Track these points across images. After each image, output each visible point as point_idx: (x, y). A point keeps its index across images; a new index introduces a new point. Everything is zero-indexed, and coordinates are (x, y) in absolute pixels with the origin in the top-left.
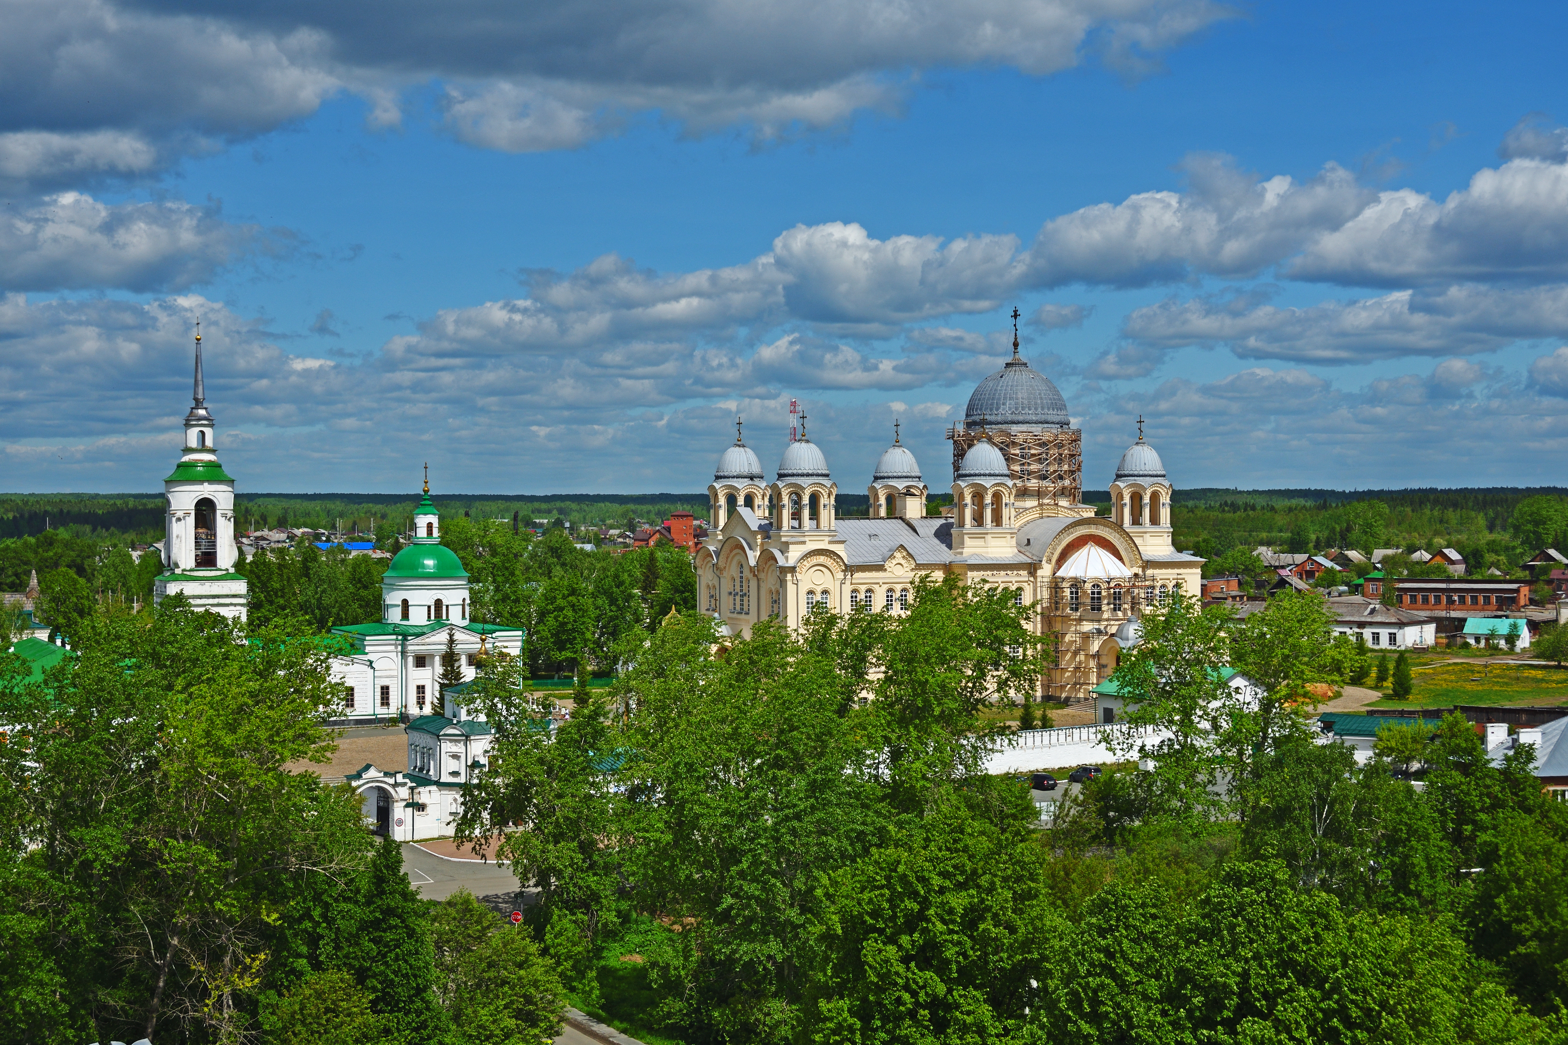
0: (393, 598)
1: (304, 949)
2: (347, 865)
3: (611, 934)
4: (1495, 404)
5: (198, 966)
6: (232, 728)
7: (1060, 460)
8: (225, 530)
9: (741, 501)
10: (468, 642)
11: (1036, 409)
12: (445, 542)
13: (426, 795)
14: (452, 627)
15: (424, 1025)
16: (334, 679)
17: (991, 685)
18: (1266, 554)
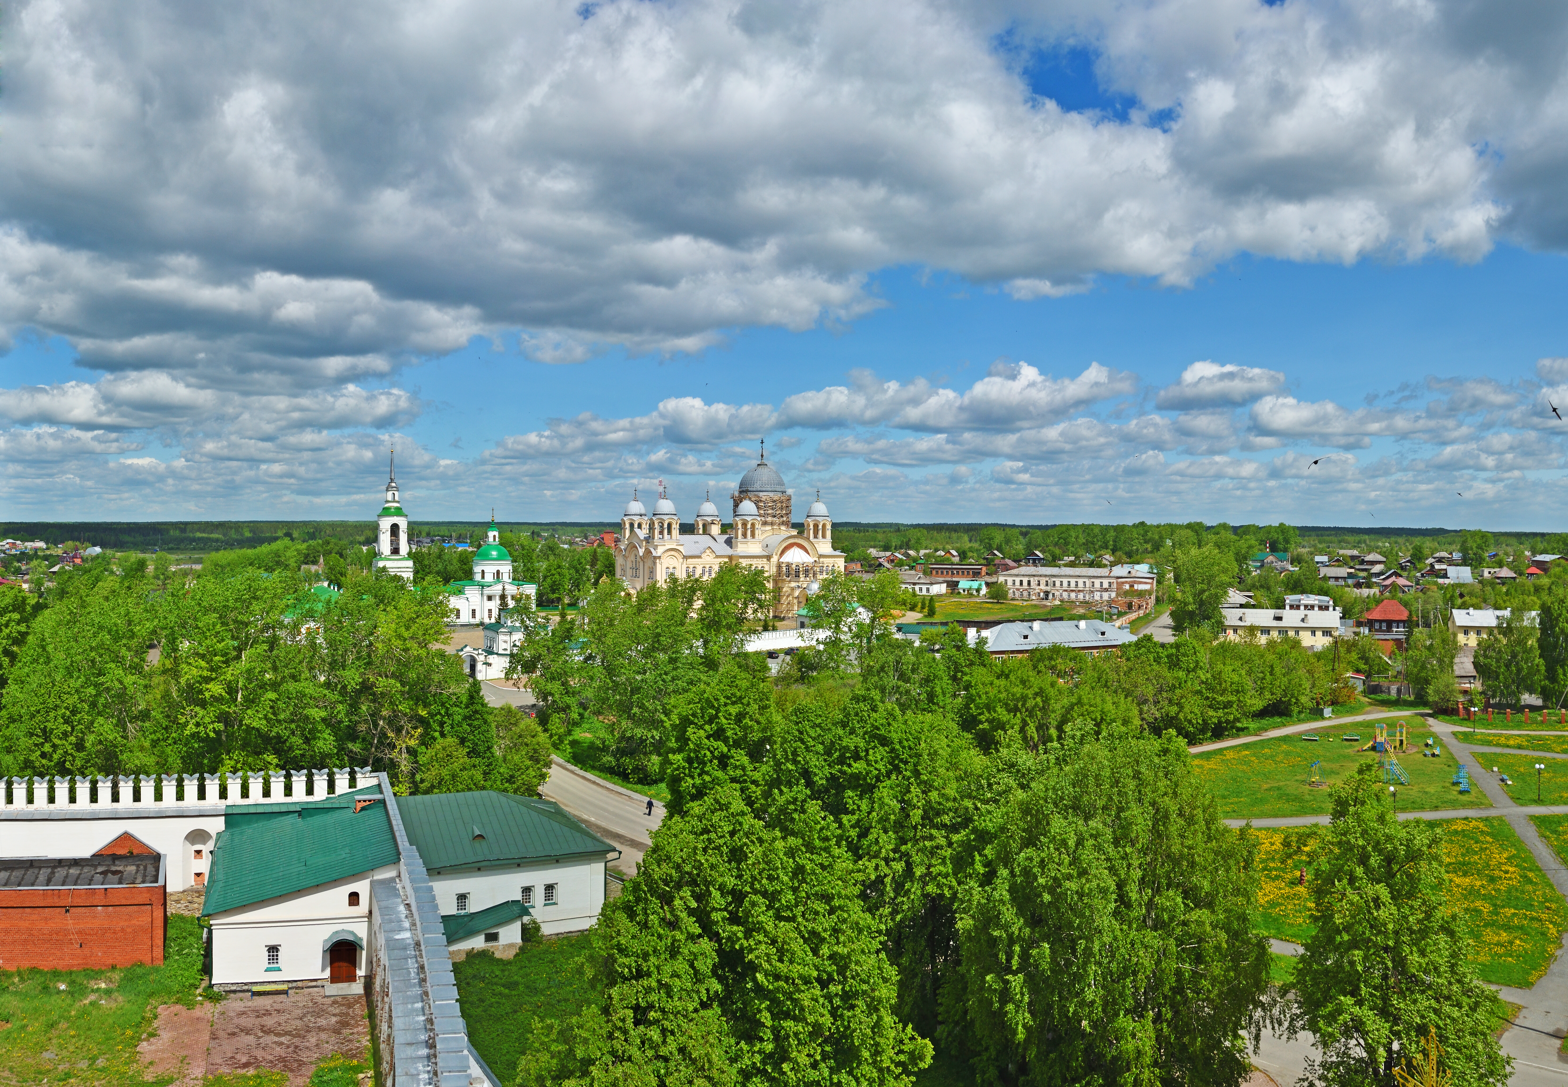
0: (477, 569)
1: (438, 728)
2: (456, 691)
3: (576, 724)
4: (977, 486)
5: (391, 734)
6: (408, 628)
7: (782, 509)
8: (403, 537)
9: (636, 526)
10: (511, 590)
12: (501, 544)
13: (492, 659)
14: (504, 583)
15: (491, 764)
16: (451, 607)
17: (750, 611)
18: (873, 552)
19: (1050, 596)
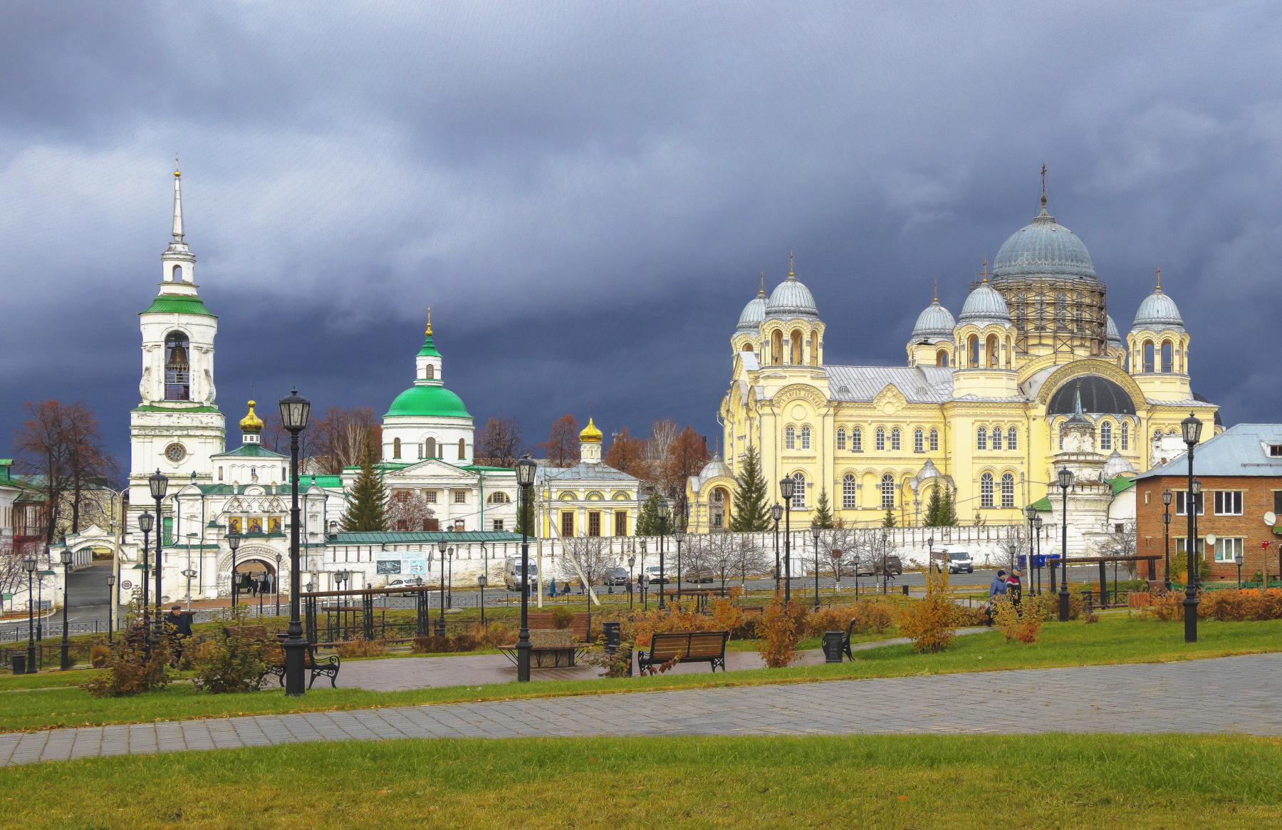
0: (388, 436)
11: (1053, 259)
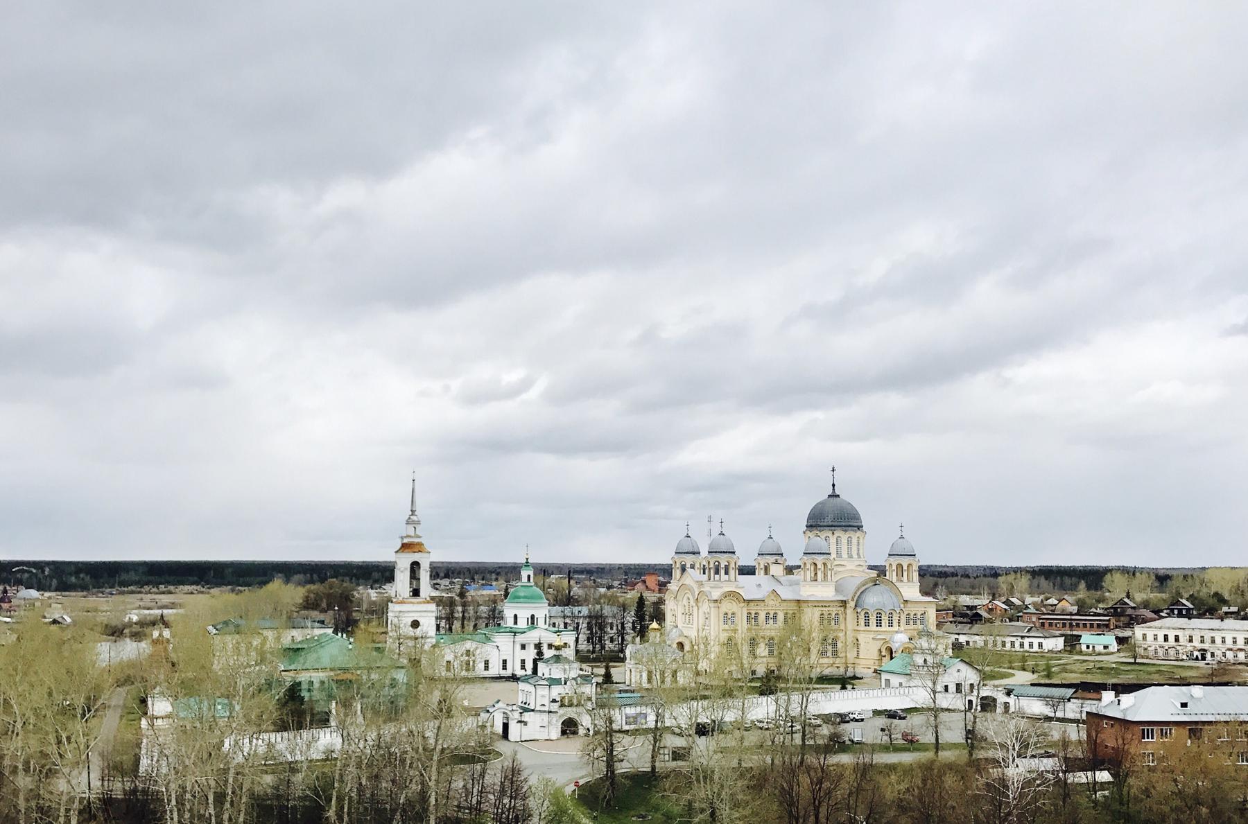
13: (527, 717)
19: (1208, 656)
